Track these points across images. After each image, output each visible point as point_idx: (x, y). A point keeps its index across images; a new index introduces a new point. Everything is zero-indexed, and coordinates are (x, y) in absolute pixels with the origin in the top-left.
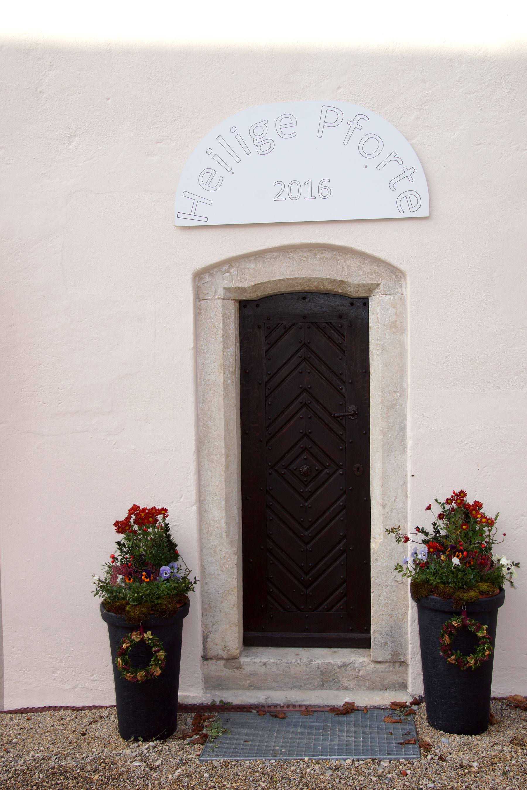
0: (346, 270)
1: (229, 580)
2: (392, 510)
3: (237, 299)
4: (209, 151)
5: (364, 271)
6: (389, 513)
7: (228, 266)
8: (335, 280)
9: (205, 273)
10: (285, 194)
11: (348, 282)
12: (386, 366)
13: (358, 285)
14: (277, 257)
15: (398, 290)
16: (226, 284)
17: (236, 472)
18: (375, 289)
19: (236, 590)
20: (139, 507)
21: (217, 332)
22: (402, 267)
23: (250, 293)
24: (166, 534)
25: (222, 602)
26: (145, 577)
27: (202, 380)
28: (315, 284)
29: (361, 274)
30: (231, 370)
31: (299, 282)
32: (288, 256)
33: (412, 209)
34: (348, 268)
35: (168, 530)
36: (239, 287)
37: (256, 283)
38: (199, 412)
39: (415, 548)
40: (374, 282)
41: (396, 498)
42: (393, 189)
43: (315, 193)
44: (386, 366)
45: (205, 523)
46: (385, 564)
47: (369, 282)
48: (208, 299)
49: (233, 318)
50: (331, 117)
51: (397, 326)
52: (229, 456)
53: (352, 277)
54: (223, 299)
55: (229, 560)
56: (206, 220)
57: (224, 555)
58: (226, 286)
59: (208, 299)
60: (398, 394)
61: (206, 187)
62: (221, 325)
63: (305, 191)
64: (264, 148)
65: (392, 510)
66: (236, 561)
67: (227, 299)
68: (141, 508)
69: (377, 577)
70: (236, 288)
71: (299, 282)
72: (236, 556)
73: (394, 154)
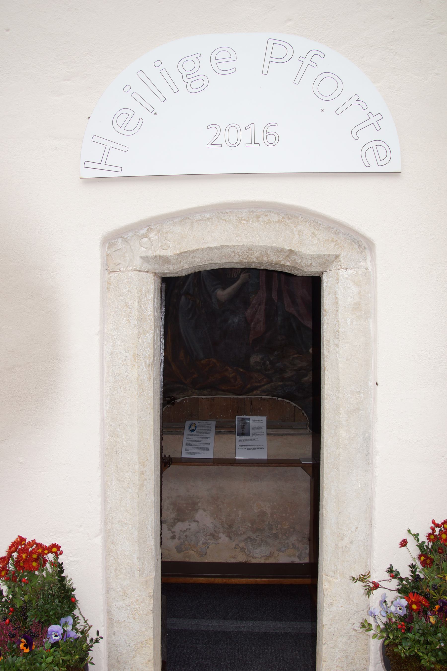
0: (297, 237)
1: (144, 629)
2: (351, 542)
3: (157, 272)
4: (127, 88)
5: (319, 239)
6: (348, 546)
7: (146, 229)
8: (282, 250)
9: (118, 238)
10: (220, 140)
11: (299, 252)
12: (347, 360)
13: (312, 256)
14: (208, 219)
15: (363, 264)
16: (143, 251)
17: (152, 493)
18: (333, 262)
19: (152, 643)
20: (25, 540)
21: (130, 313)
22: (369, 233)
23: (174, 264)
24: (59, 576)
25: (134, 657)
26: (25, 646)
27: (110, 374)
28: (257, 254)
29: (315, 242)
30: (148, 362)
31: (236, 251)
32: (223, 218)
33: (381, 163)
34: (299, 235)
35: (62, 571)
36: (160, 256)
37: (182, 250)
38: (105, 415)
39: (389, 600)
40: (332, 253)
41: (357, 528)
42: (357, 138)
43: (259, 139)
44: (347, 360)
45: (112, 558)
46: (341, 609)
47: (326, 253)
48: (120, 271)
49: (152, 295)
50: (279, 51)
51: (364, 309)
52: (143, 473)
53: (300, 249)
54: (140, 271)
55: (143, 605)
56: (119, 170)
57: (137, 598)
58: (144, 255)
59: (120, 271)
60: (362, 395)
61: (121, 130)
62: (136, 304)
63: (246, 139)
64: (196, 85)
65: (351, 542)
66: (151, 607)
67: (144, 271)
68: (27, 541)
69: (331, 625)
70: (156, 257)
71: (236, 251)
72: (152, 600)
73: (356, 97)
